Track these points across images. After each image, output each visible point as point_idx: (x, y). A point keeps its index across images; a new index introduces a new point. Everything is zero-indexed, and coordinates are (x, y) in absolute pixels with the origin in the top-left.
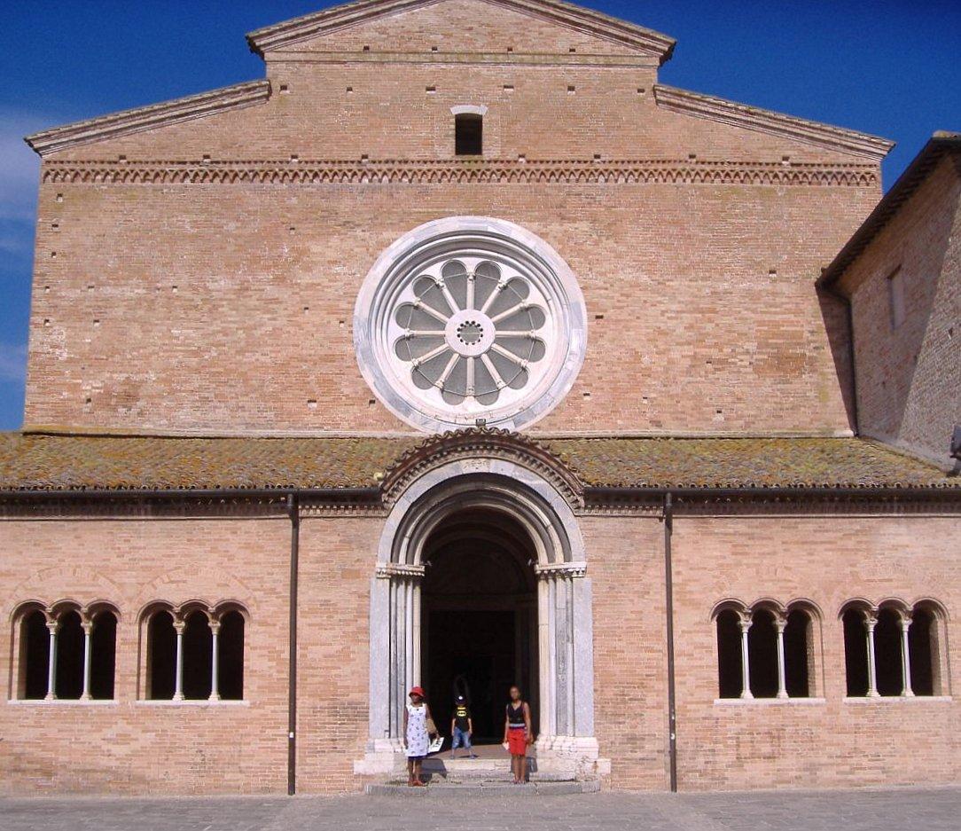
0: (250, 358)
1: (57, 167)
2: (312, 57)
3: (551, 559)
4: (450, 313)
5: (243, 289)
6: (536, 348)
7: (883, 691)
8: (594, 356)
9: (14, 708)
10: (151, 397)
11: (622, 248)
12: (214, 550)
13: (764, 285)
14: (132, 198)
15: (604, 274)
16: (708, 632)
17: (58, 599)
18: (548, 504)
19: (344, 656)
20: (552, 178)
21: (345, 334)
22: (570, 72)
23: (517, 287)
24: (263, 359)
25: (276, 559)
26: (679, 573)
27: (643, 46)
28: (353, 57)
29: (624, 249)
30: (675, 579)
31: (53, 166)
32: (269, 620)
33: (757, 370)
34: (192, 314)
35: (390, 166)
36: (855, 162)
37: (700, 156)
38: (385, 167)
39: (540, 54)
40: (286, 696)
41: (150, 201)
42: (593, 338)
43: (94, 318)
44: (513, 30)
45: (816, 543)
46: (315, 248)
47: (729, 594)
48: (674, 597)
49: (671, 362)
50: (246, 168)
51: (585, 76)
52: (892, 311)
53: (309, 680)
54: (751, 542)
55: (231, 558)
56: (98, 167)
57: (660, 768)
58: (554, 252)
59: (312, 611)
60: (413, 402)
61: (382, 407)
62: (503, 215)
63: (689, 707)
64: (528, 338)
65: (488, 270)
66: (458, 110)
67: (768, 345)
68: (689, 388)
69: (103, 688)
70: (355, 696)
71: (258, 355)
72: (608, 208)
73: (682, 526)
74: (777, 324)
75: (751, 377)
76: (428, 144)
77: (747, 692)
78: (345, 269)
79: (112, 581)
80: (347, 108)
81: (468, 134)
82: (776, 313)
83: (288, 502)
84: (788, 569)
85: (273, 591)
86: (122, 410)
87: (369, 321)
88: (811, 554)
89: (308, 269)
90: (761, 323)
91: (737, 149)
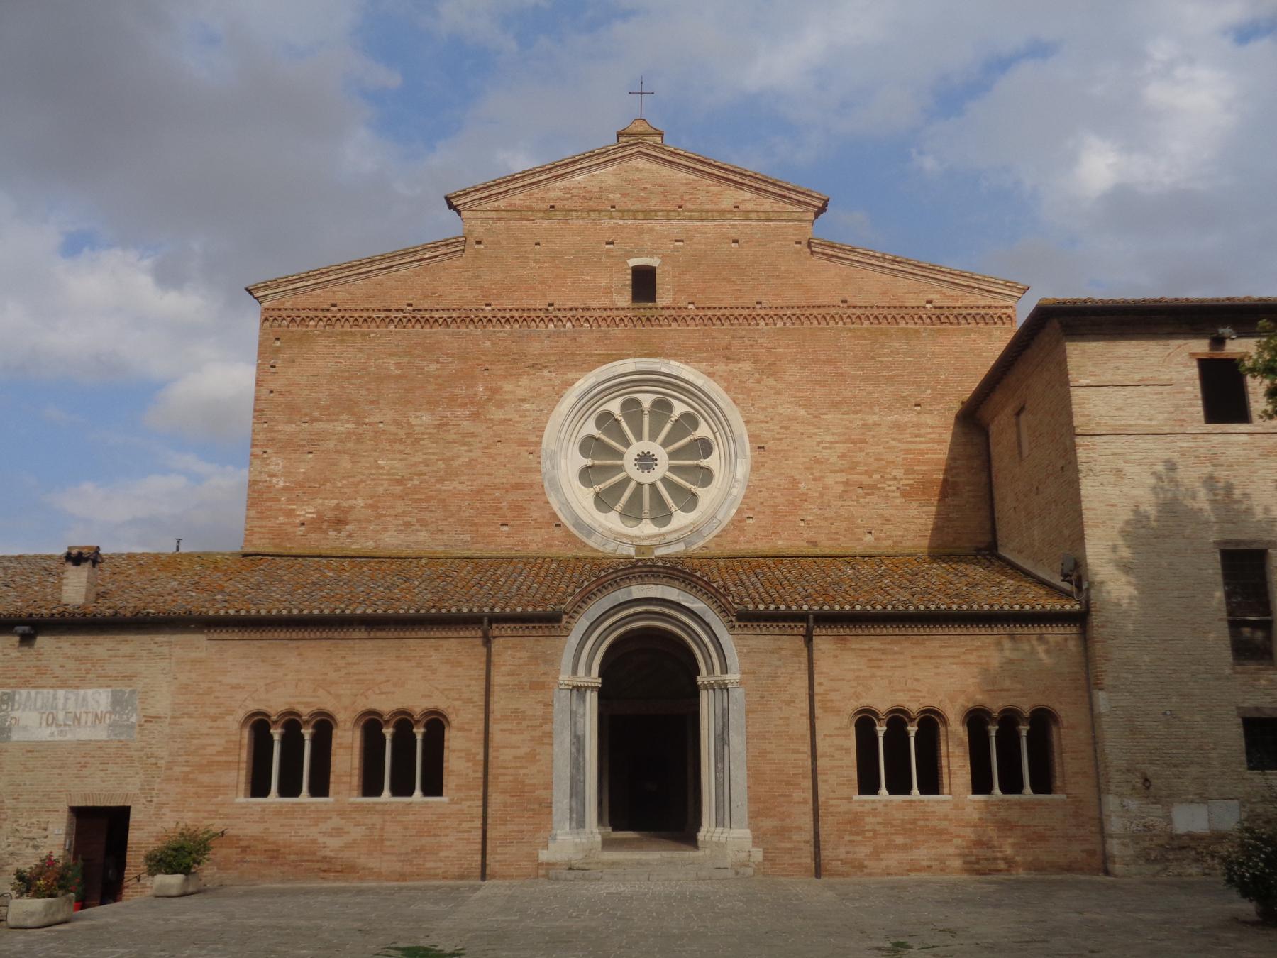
0: (449, 486)
1: (275, 313)
2: (504, 215)
3: (711, 671)
4: (627, 444)
5: (443, 424)
6: (706, 476)
7: (892, 791)
8: (757, 483)
9: (242, 806)
10: (359, 521)
11: (781, 386)
12: (419, 665)
13: (910, 417)
14: (343, 341)
15: (764, 409)
16: (847, 736)
17: (282, 708)
18: (708, 625)
19: (532, 757)
20: (721, 325)
21: (534, 465)
22: (735, 226)
23: (689, 421)
24: (460, 487)
25: (472, 672)
26: (820, 684)
27: (799, 202)
28: (540, 215)
29: (783, 386)
30: (817, 689)
31: (272, 313)
32: (466, 727)
33: (905, 494)
34: (397, 446)
35: (574, 312)
36: (993, 304)
37: (851, 301)
38: (569, 314)
39: (707, 211)
40: (480, 793)
41: (359, 345)
42: (755, 467)
43: (307, 449)
44: (683, 189)
45: (940, 657)
46: (508, 387)
47: (866, 702)
48: (817, 705)
49: (826, 487)
50: (445, 315)
51: (748, 230)
52: (1020, 445)
53: (501, 779)
54: (883, 657)
55: (434, 672)
56: (312, 314)
57: (55, 698)
58: (720, 390)
59: (505, 718)
60: (596, 526)
61: (567, 530)
62: (675, 356)
63: (831, 802)
64: (697, 466)
65: (662, 407)
66: (634, 262)
67: (914, 472)
68: (842, 512)
69: (320, 787)
70: (541, 793)
71: (456, 484)
72: (769, 349)
73: (824, 643)
74: (922, 453)
75: (898, 501)
76: (607, 292)
77: (883, 790)
78: (534, 407)
79: (330, 693)
80: (536, 261)
81: (644, 283)
82: (921, 442)
83: (482, 624)
84: (918, 680)
85: (470, 701)
86: (332, 533)
87: (563, 425)
88: (937, 667)
89: (500, 406)
90: (907, 452)
91: (885, 294)
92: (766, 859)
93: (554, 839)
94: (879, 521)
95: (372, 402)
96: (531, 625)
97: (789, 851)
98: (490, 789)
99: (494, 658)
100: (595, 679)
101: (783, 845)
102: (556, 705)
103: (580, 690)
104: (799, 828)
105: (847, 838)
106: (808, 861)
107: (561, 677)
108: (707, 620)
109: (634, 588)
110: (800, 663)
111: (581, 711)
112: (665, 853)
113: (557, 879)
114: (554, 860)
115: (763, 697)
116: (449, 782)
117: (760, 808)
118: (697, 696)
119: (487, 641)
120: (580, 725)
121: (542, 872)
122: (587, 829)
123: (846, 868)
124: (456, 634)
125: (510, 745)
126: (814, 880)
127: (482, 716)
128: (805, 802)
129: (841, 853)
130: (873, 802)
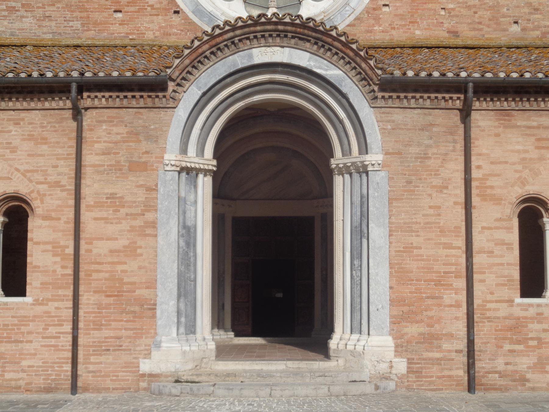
3: (347, 152)
16: (509, 229)
19: (131, 251)
25: (60, 151)
26: (479, 167)
30: (475, 174)
32: (53, 214)
40: (70, 293)
53: (95, 276)
55: (14, 150)
59: (99, 205)
61: (186, 18)
63: (489, 306)
73: (484, 118)
85: (57, 184)
92: (410, 371)
93: (158, 346)
94: (526, 10)
96: (130, 94)
97: (437, 361)
98: (82, 288)
99: (86, 134)
100: (208, 159)
101: (431, 355)
102: (161, 189)
103: (190, 172)
104: (451, 336)
105: (507, 347)
106: (461, 373)
107: (167, 157)
108: (344, 90)
109: (255, 51)
110: (455, 142)
111: (192, 197)
112: (290, 364)
113: (160, 393)
114: (156, 371)
115: (409, 182)
116: (33, 280)
117: (405, 312)
118: (327, 194)
119: (77, 114)
120: (190, 214)
121: (143, 385)
122: (199, 335)
123: (502, 382)
124: (40, 105)
125: (104, 236)
126: (466, 394)
127: (72, 202)
128: (458, 305)
129: (500, 364)
130: (539, 305)
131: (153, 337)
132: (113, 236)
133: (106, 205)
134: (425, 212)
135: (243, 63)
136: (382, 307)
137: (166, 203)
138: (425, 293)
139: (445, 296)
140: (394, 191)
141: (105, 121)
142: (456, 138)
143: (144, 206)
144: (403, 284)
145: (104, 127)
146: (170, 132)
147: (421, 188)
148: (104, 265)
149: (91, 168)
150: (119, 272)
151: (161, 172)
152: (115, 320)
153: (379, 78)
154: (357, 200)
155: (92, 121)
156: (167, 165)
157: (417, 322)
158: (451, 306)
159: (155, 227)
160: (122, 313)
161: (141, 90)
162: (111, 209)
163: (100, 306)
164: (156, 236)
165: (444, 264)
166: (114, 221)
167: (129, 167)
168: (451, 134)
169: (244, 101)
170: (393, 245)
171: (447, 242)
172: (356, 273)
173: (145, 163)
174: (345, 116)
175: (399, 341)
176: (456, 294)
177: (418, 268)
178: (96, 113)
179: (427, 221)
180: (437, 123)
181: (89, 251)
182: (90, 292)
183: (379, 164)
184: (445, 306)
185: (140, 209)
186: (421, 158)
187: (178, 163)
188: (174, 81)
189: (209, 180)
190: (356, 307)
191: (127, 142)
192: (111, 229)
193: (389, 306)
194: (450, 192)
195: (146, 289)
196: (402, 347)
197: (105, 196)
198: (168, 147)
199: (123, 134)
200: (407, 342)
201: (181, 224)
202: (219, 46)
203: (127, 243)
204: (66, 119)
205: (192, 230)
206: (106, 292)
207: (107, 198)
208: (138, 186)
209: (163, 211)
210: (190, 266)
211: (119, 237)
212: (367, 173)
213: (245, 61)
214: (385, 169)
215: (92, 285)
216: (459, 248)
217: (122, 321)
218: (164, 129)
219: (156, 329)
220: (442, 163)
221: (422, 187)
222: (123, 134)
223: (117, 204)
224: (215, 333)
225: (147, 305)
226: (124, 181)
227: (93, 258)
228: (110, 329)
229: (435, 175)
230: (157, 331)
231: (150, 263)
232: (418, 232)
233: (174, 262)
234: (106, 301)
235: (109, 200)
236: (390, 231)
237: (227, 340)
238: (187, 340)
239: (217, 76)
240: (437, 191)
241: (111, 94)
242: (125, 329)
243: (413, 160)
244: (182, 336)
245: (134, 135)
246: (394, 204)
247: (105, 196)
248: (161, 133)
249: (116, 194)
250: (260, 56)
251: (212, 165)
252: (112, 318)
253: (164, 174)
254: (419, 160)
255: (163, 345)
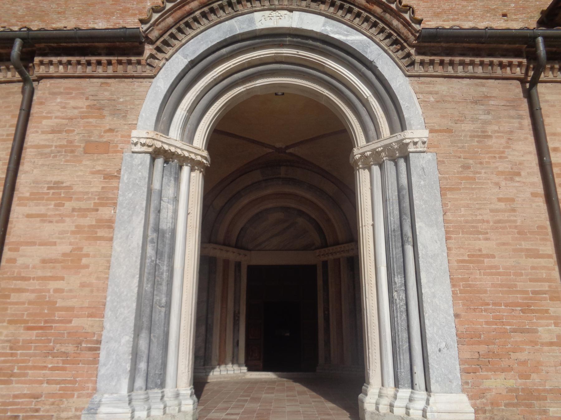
53: (14, 297)
59: (36, 197)
95: (59, 13)
96: (93, 59)
102: (125, 176)
107: (134, 133)
110: (520, 117)
111: (169, 192)
115: (466, 167)
122: (169, 391)
131: (90, 396)
132: (51, 240)
133: (46, 197)
134: (493, 206)
135: (243, 28)
136: (446, 346)
137: (130, 195)
138: (509, 324)
139: (540, 329)
140: (446, 179)
141: (60, 93)
142: (521, 113)
143: (98, 199)
144: (474, 310)
145: (59, 100)
146: (144, 106)
147: (483, 175)
148: (31, 281)
149: (33, 150)
150: (51, 291)
151: (127, 155)
152: (34, 368)
153: (417, 35)
154: (393, 194)
155: (44, 93)
156: (136, 144)
157: (503, 370)
158: (551, 344)
159: (111, 227)
160: (46, 355)
161: (110, 52)
162: (53, 203)
163: (14, 345)
164: (111, 239)
165: (531, 280)
166: (55, 219)
167: (84, 148)
168: (514, 107)
169: (244, 86)
170: (453, 252)
171: (531, 247)
172: (399, 296)
173: (108, 143)
174: (371, 94)
175: (478, 402)
176: (556, 325)
177: (493, 285)
178: (51, 84)
179: (498, 218)
180: (494, 95)
181: (13, 261)
182: (4, 322)
183: (424, 143)
184: (543, 344)
185: (92, 202)
186: (478, 136)
187: (149, 142)
188: (152, 42)
189: (197, 177)
190: (403, 346)
191: (87, 117)
192: (48, 230)
193: (456, 345)
194: (524, 180)
195: (88, 317)
196: (485, 412)
197: (46, 186)
198: (139, 123)
199: (82, 108)
200: (492, 404)
201: (151, 225)
202: (212, 5)
203: (67, 249)
204: (14, 93)
205: (168, 235)
206: (26, 322)
207: (49, 188)
208: (93, 173)
209: (125, 205)
210: (161, 284)
211: (58, 241)
212: (407, 159)
213: (245, 26)
214: (431, 150)
215: (9, 312)
216: (549, 256)
217: (45, 368)
218: (137, 102)
219: (96, 382)
220: (507, 143)
221: (485, 173)
222: (82, 108)
223: (63, 195)
224: (229, 369)
225: (87, 342)
226: (76, 166)
227: (16, 271)
228: (25, 382)
229: (500, 158)
230: (98, 385)
231: (98, 278)
232: (487, 233)
233: (134, 277)
234: (24, 335)
235: (52, 191)
236: (447, 232)
237: (240, 375)
238: (147, 399)
239: (209, 43)
240: (506, 179)
241: (70, 58)
242: (48, 382)
243: (468, 139)
244: (140, 392)
245: (97, 109)
246: (448, 196)
247: (46, 186)
248: (132, 107)
249: (62, 183)
250: (263, 21)
251: (202, 156)
252: (30, 364)
253: (131, 157)
254: (476, 139)
255: (103, 409)
